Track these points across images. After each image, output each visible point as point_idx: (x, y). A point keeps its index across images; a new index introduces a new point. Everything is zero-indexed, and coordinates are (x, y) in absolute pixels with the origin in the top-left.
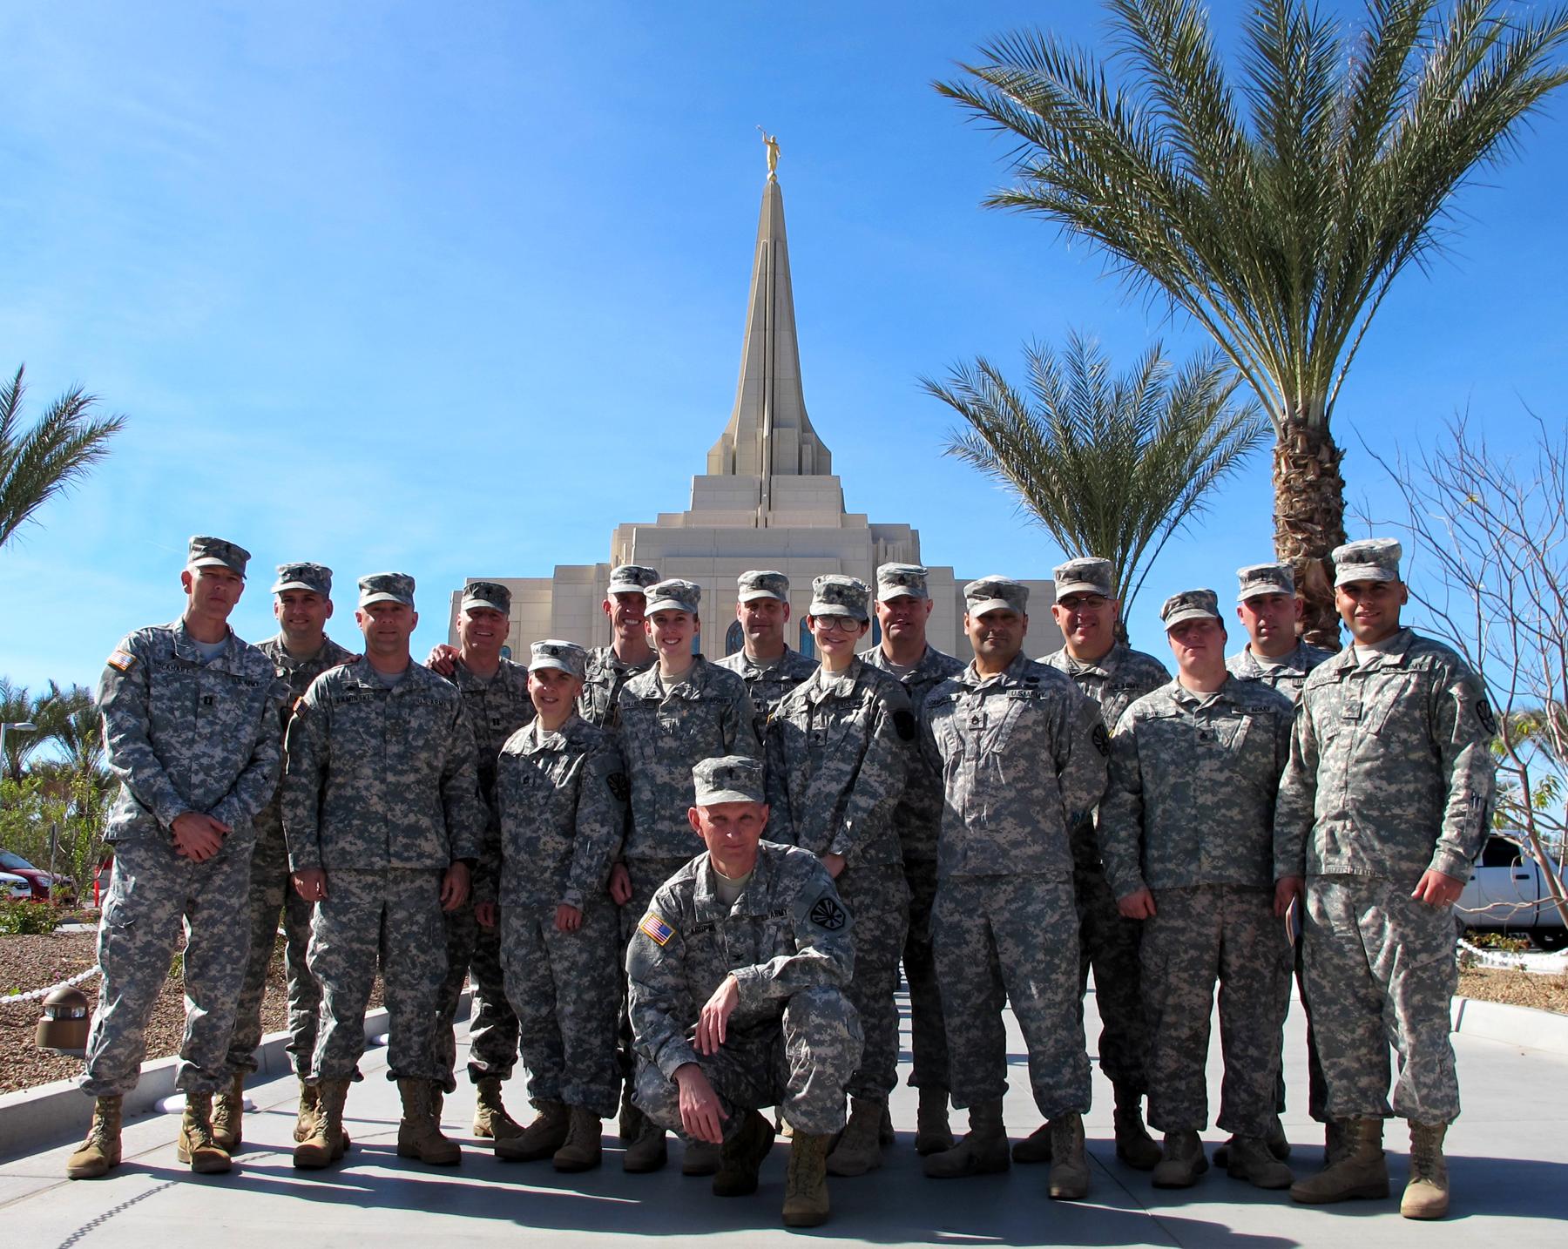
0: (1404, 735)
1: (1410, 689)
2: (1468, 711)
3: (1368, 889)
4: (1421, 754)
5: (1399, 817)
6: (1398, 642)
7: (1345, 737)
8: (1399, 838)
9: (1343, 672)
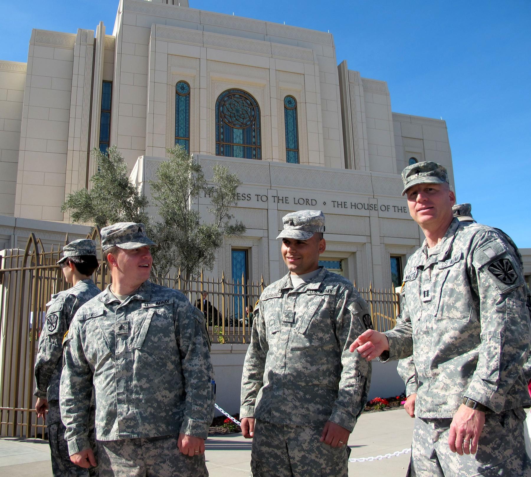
0: (320, 335)
1: (325, 305)
2: (358, 320)
3: (295, 432)
4: (331, 346)
5: (317, 386)
6: (317, 275)
7: (284, 334)
8: (318, 399)
9: (284, 291)
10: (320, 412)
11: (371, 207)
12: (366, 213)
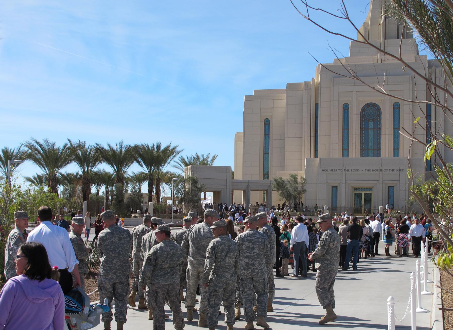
10: (39, 180)
11: (379, 170)
12: (378, 173)
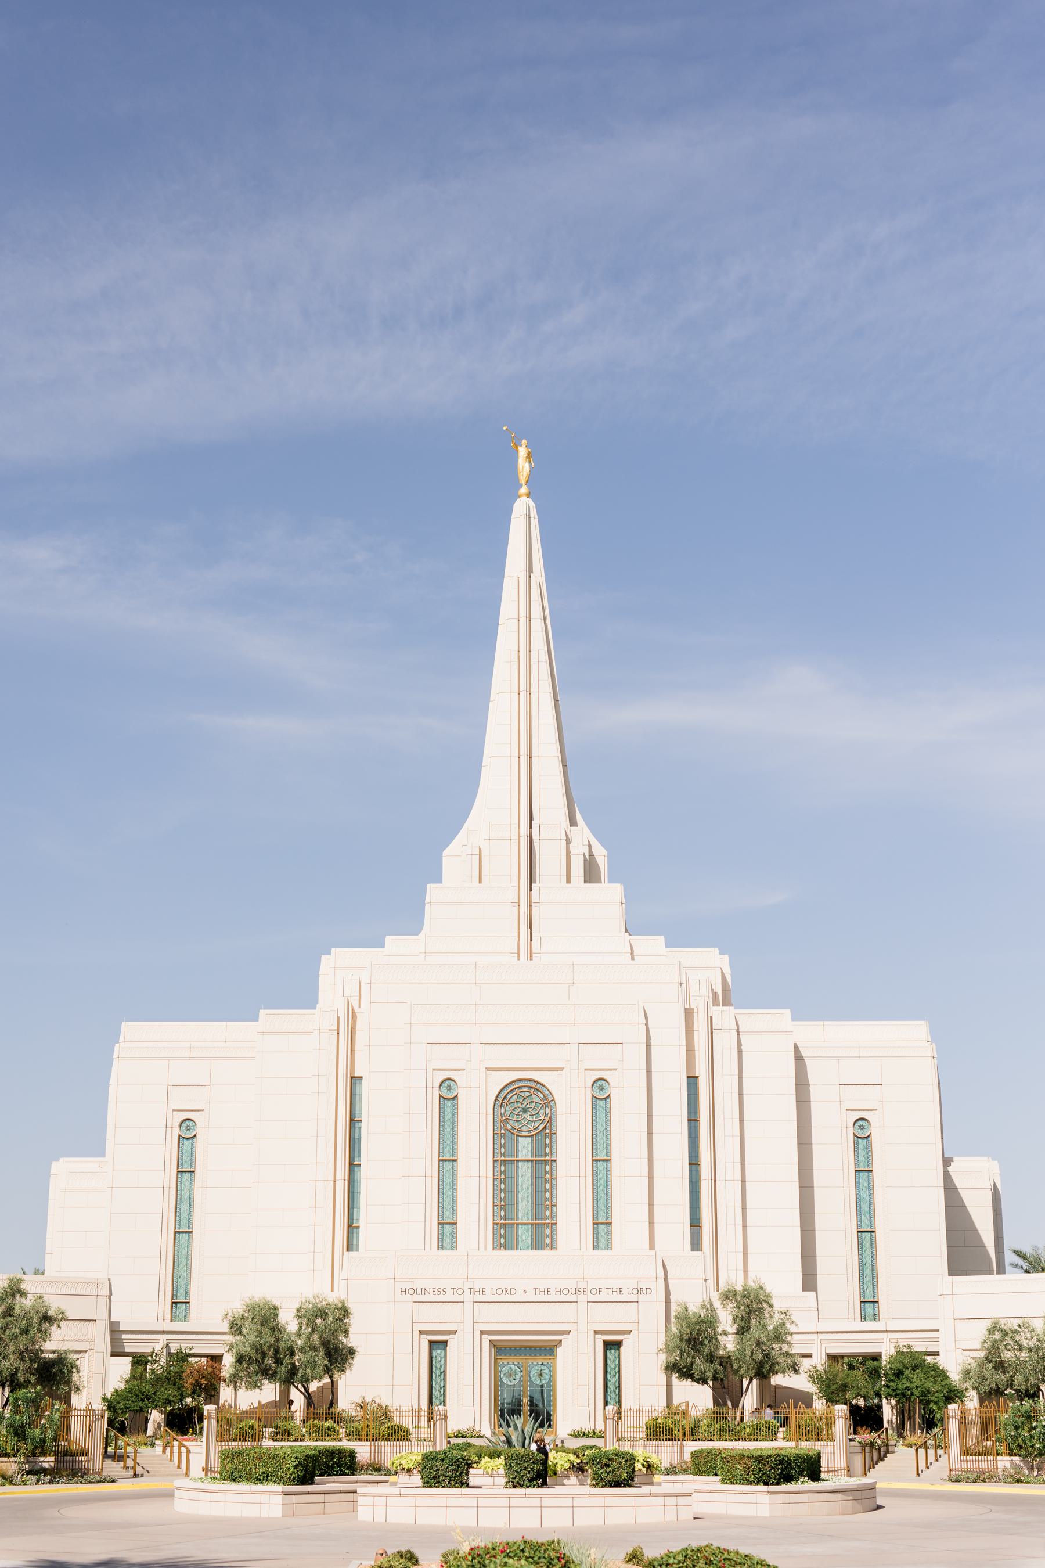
12: (573, 1298)
